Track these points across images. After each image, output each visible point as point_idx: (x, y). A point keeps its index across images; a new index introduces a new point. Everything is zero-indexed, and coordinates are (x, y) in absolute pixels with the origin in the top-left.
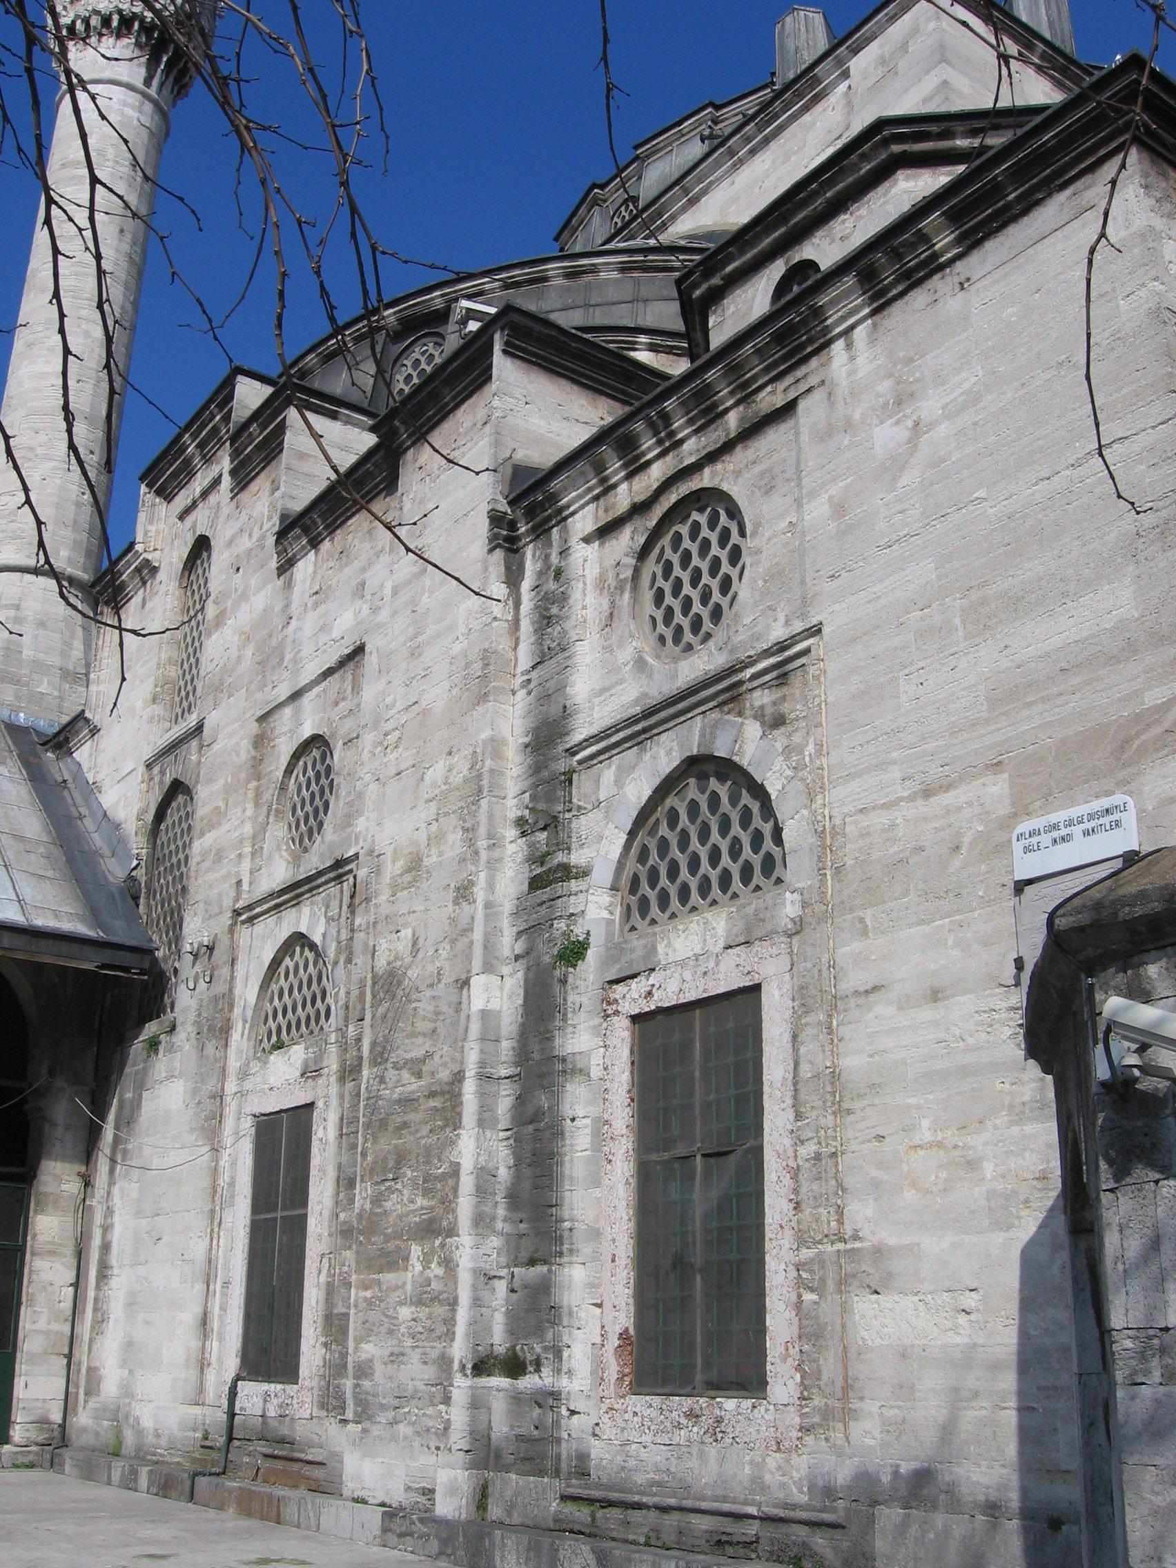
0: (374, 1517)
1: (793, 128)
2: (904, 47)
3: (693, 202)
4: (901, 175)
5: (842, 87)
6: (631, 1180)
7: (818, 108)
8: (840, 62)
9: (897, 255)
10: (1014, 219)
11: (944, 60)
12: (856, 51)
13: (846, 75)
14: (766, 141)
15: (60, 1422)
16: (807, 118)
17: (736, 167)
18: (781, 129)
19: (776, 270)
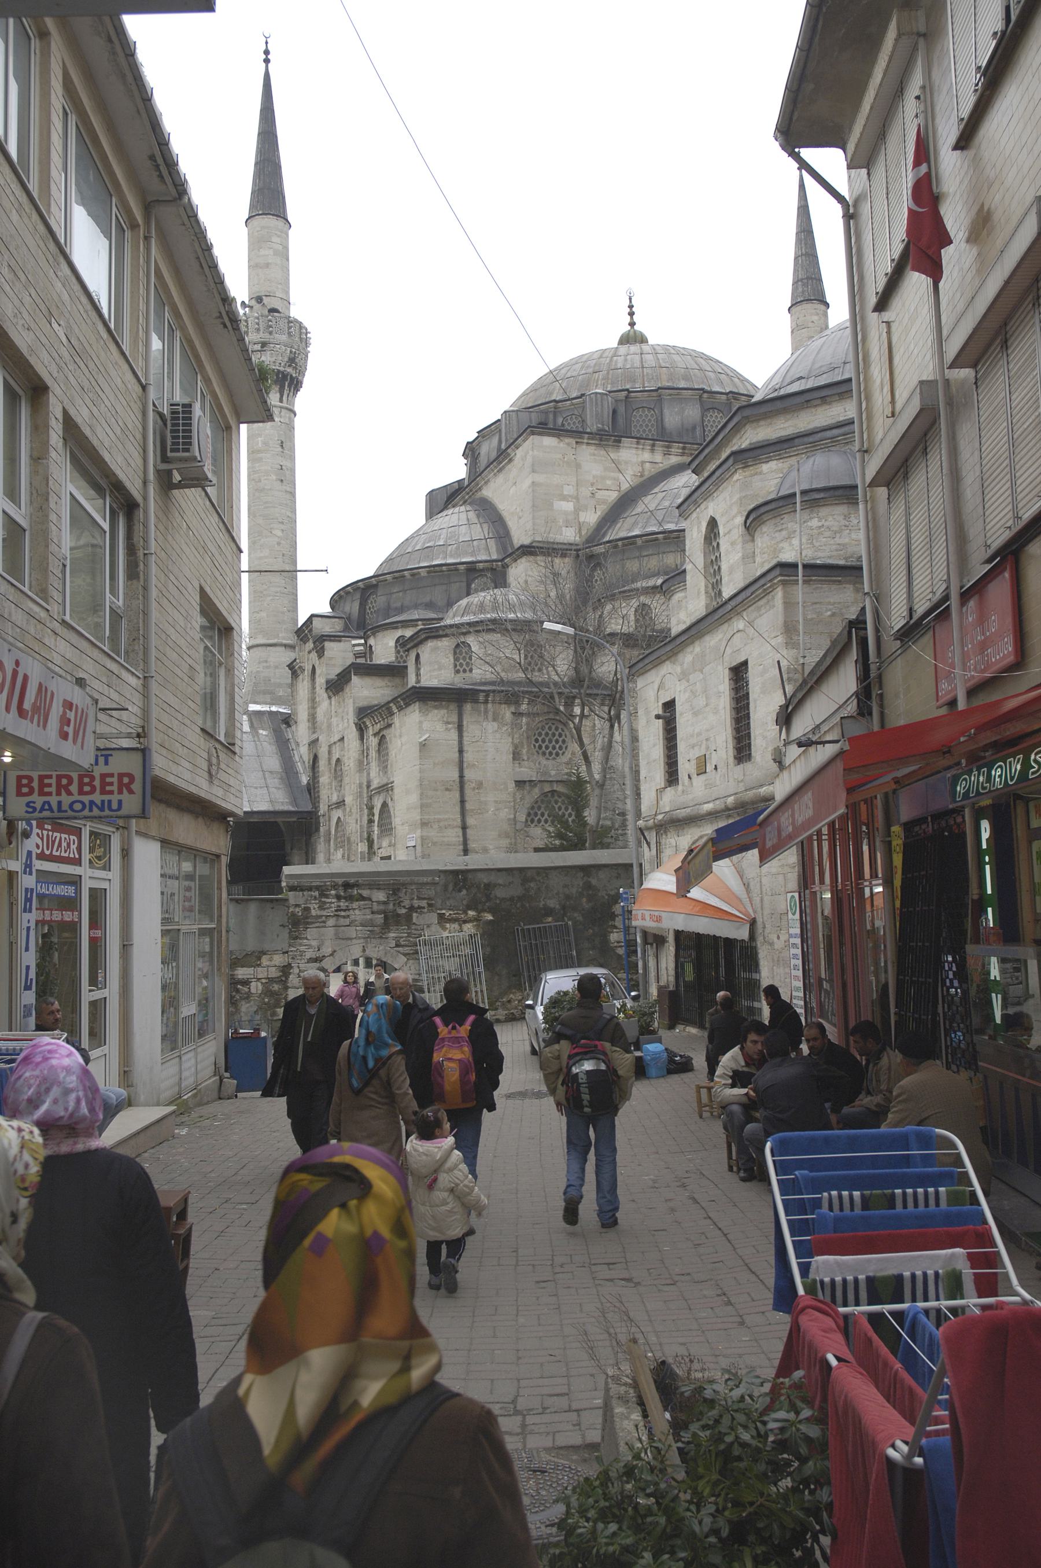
16: (509, 466)
18: (504, 467)
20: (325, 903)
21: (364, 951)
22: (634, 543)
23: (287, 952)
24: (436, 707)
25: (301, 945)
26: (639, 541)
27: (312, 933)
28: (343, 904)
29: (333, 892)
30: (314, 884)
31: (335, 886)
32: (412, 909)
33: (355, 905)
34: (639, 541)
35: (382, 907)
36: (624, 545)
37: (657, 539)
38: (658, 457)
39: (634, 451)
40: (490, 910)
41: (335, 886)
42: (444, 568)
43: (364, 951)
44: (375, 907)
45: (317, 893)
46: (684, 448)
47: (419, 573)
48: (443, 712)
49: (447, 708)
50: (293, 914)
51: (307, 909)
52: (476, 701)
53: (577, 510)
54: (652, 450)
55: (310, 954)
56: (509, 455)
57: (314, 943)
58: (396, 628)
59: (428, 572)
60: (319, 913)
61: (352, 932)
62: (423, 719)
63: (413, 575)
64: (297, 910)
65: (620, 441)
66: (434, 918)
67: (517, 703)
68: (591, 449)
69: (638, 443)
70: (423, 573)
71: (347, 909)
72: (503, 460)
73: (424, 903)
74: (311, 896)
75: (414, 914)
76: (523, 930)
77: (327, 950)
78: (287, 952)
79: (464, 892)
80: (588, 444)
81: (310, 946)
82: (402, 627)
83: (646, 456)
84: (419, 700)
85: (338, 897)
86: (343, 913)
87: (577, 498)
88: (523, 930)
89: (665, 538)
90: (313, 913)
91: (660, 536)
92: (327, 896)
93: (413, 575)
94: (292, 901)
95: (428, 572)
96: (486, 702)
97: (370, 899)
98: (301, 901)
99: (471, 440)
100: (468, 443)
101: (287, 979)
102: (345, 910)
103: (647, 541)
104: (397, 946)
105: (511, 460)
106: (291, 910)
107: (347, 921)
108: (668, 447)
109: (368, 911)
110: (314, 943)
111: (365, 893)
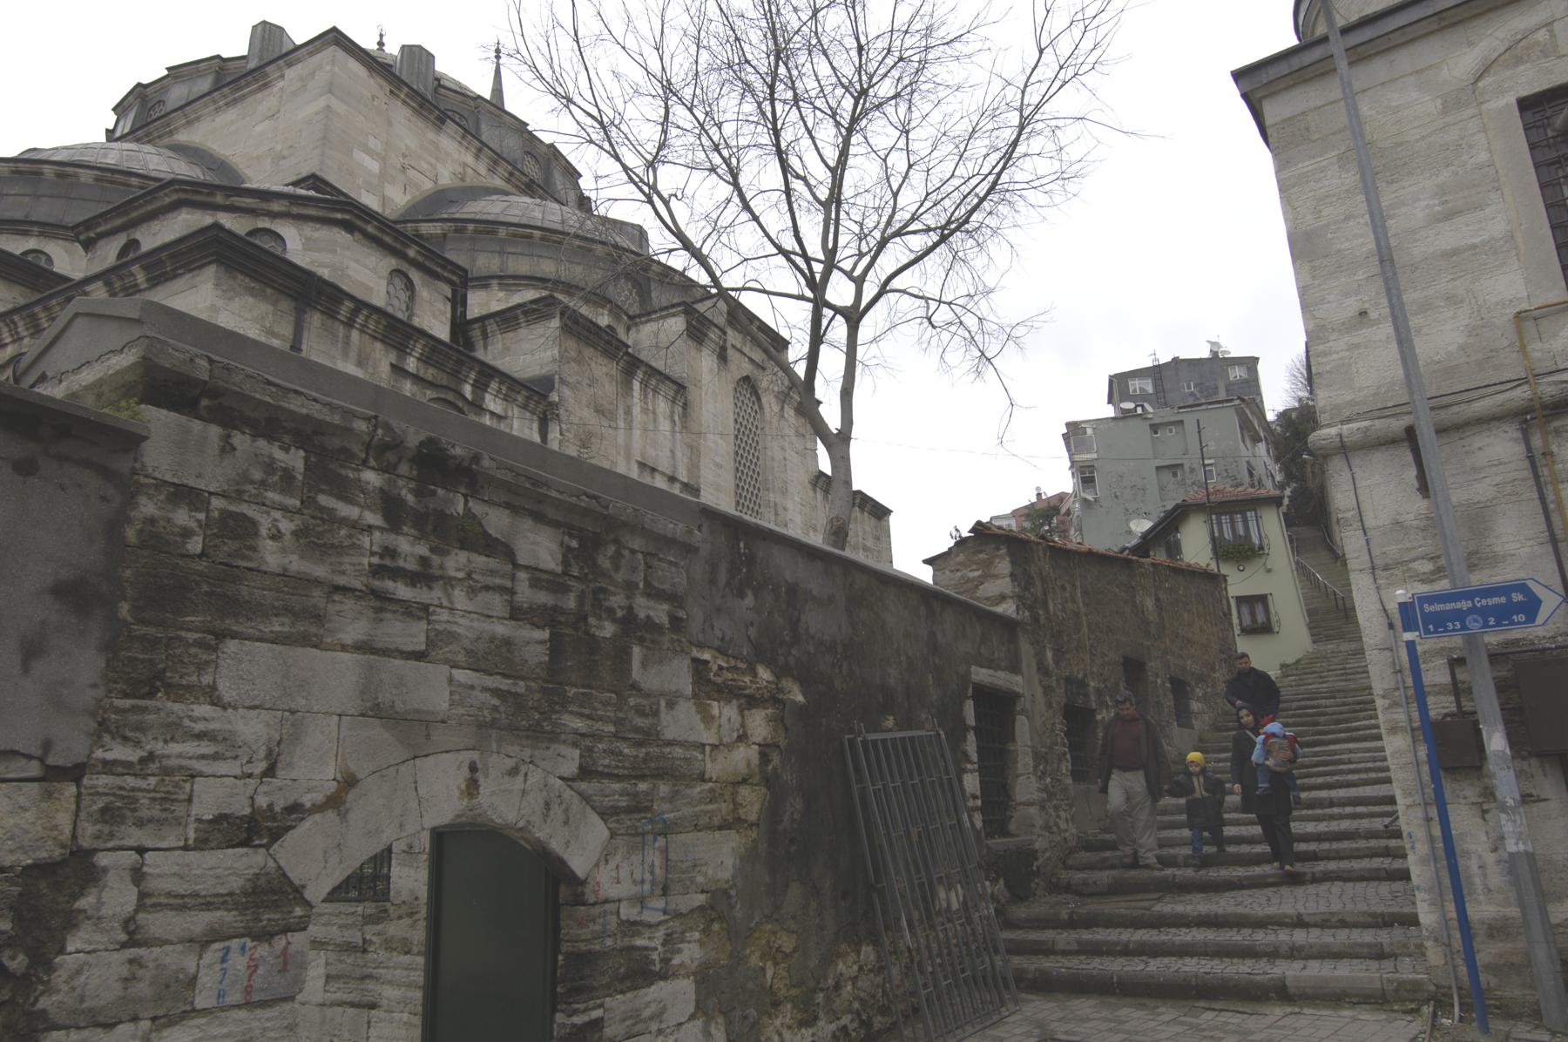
0: (360, 776)
1: (251, 99)
2: (313, 74)
3: (189, 123)
4: (184, 210)
5: (281, 84)
6: (802, 430)
7: (266, 92)
8: (280, 69)
9: (121, 278)
10: (167, 280)
11: (330, 92)
12: (289, 65)
13: (282, 76)
14: (235, 101)
15: (1511, 431)
16: (259, 95)
17: (218, 110)
18: (244, 97)
19: (120, 241)
20: (330, 518)
21: (472, 787)
22: (494, 232)
23: (75, 773)
24: (251, 292)
25: (174, 730)
26: (502, 232)
27: (246, 666)
28: (410, 548)
29: (371, 478)
30: (295, 405)
31: (384, 451)
32: (630, 625)
33: (456, 562)
34: (502, 232)
35: (544, 598)
36: (476, 231)
37: (530, 237)
38: (483, 170)
39: (456, 145)
40: (805, 683)
41: (384, 451)
42: (134, 181)
43: (472, 787)
44: (526, 594)
45: (295, 460)
46: (511, 174)
47: (76, 176)
48: (265, 308)
49: (275, 303)
50: (156, 540)
51: (239, 529)
52: (331, 314)
53: (383, 176)
54: (477, 157)
55: (216, 794)
56: (267, 75)
57: (253, 729)
58: (26, 233)
59: (97, 179)
60: (296, 564)
61: (432, 688)
62: (220, 303)
63: (61, 176)
64: (182, 517)
65: (443, 122)
66: (678, 675)
67: (403, 350)
68: (407, 112)
69: (463, 137)
70: (86, 176)
71: (423, 576)
72: (248, 85)
73: (660, 612)
74: (270, 466)
75: (637, 651)
76: (865, 742)
77: (311, 774)
78: (75, 773)
79: (749, 600)
80: (404, 102)
81: (224, 743)
82: (41, 234)
83: (469, 159)
84: (219, 262)
85: (392, 509)
86: (403, 591)
87: (384, 159)
88: (865, 742)
89: (542, 239)
90: (272, 556)
91: (537, 233)
92: (344, 490)
93: (61, 176)
94: (158, 458)
95: (97, 179)
96: (349, 324)
97: (509, 554)
98: (212, 476)
99: (145, 81)
100: (139, 85)
101: (42, 961)
102: (413, 579)
103: (515, 236)
104: (585, 772)
105: (266, 86)
106: (147, 507)
107: (414, 635)
108: (495, 162)
109: (497, 603)
110: (253, 729)
111: (496, 521)
